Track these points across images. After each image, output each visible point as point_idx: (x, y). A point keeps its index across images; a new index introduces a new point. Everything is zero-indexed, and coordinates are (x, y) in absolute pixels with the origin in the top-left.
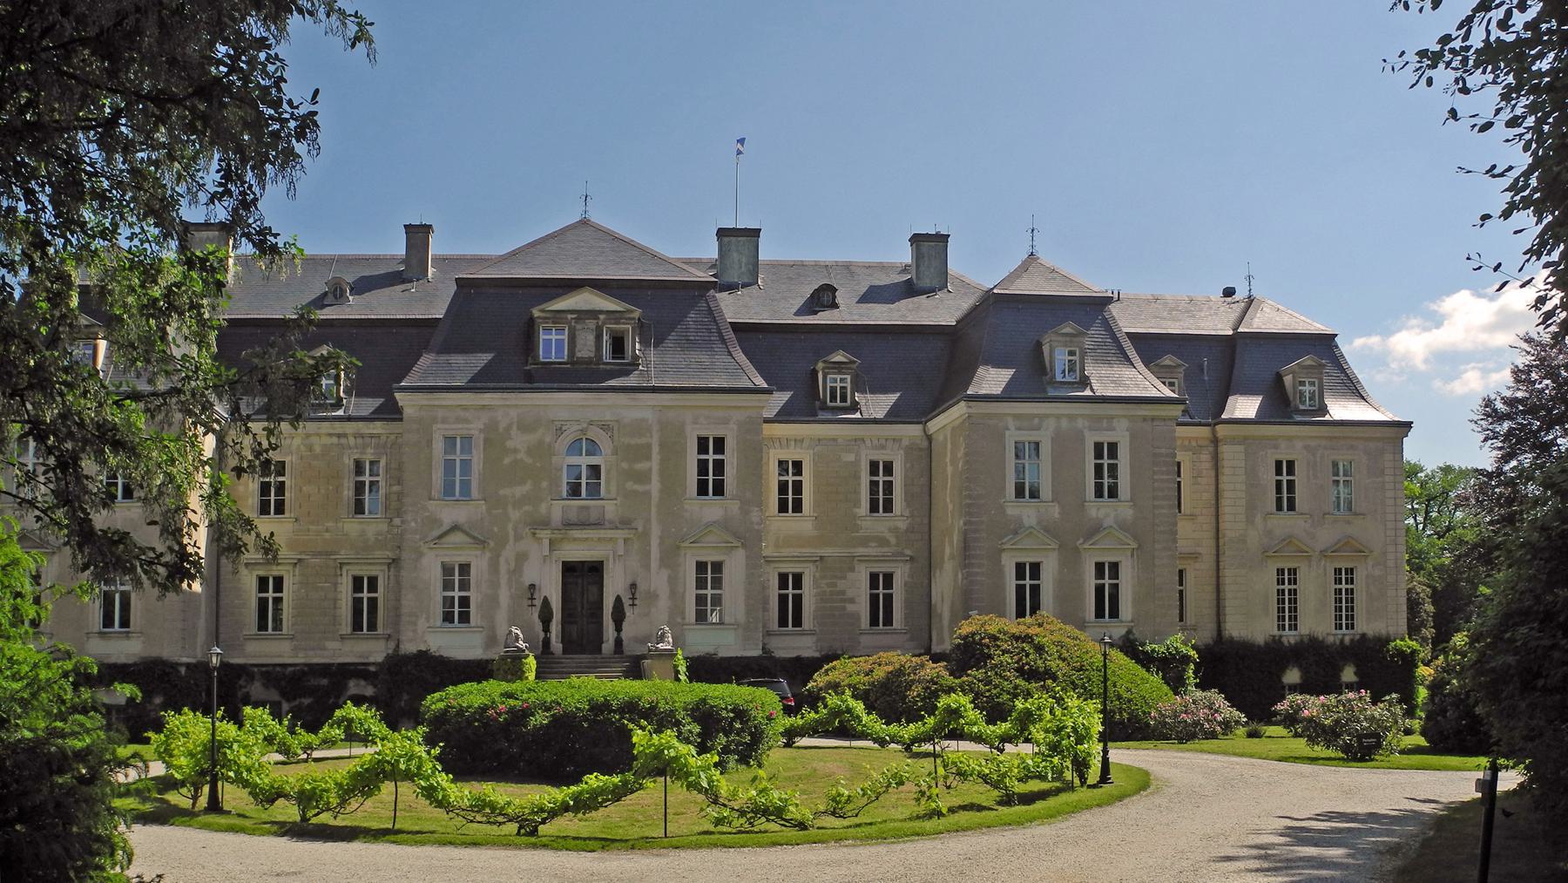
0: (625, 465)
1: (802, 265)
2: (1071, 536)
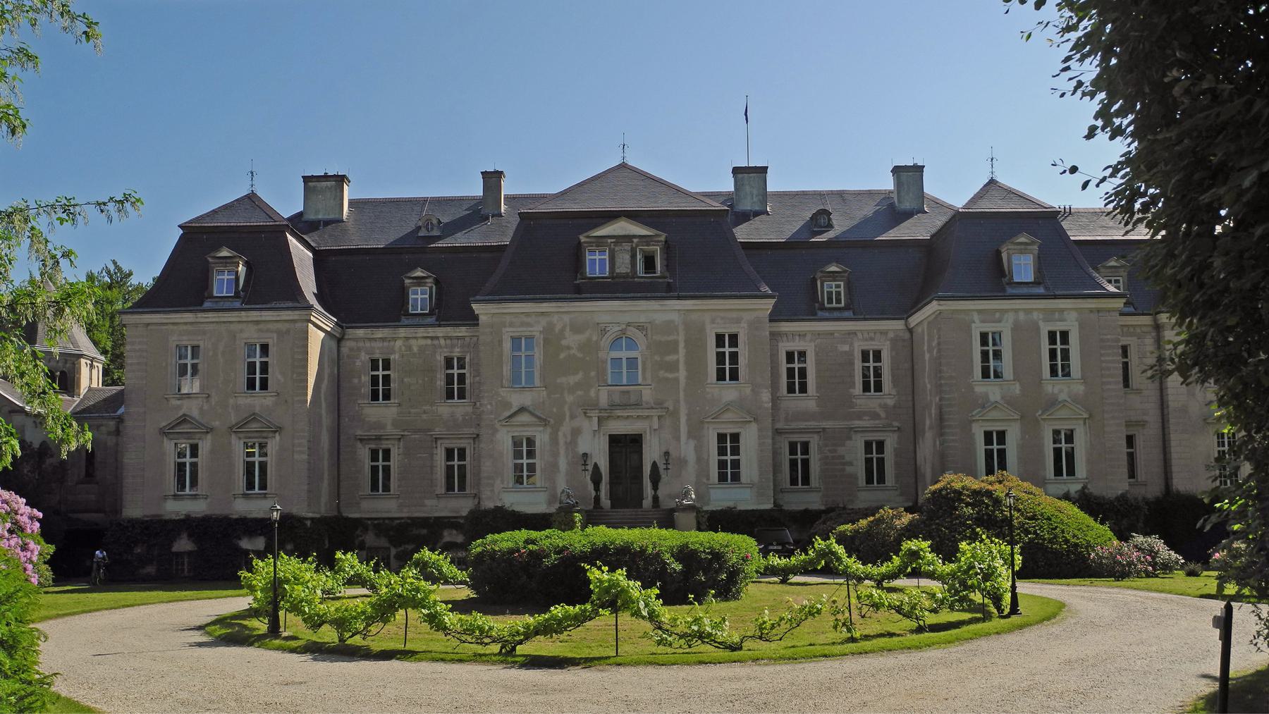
0: (657, 358)
1: (804, 194)
2: (1031, 409)
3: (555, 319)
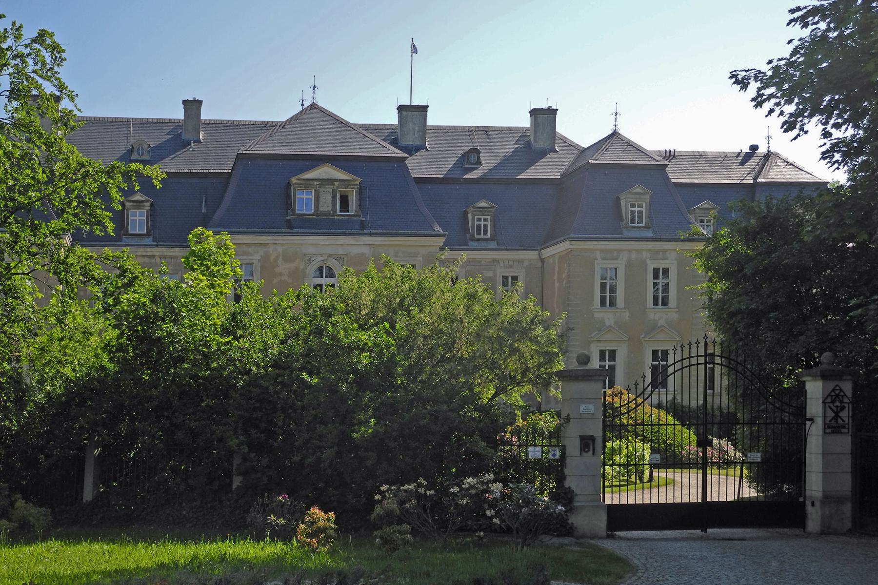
3: (271, 250)
